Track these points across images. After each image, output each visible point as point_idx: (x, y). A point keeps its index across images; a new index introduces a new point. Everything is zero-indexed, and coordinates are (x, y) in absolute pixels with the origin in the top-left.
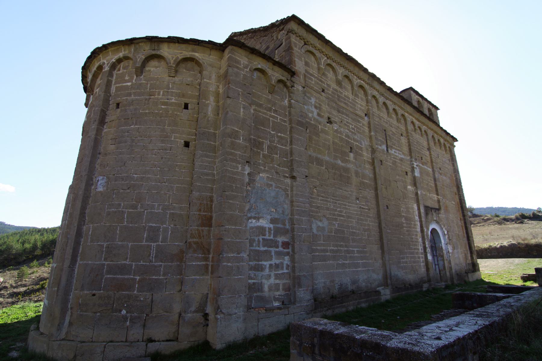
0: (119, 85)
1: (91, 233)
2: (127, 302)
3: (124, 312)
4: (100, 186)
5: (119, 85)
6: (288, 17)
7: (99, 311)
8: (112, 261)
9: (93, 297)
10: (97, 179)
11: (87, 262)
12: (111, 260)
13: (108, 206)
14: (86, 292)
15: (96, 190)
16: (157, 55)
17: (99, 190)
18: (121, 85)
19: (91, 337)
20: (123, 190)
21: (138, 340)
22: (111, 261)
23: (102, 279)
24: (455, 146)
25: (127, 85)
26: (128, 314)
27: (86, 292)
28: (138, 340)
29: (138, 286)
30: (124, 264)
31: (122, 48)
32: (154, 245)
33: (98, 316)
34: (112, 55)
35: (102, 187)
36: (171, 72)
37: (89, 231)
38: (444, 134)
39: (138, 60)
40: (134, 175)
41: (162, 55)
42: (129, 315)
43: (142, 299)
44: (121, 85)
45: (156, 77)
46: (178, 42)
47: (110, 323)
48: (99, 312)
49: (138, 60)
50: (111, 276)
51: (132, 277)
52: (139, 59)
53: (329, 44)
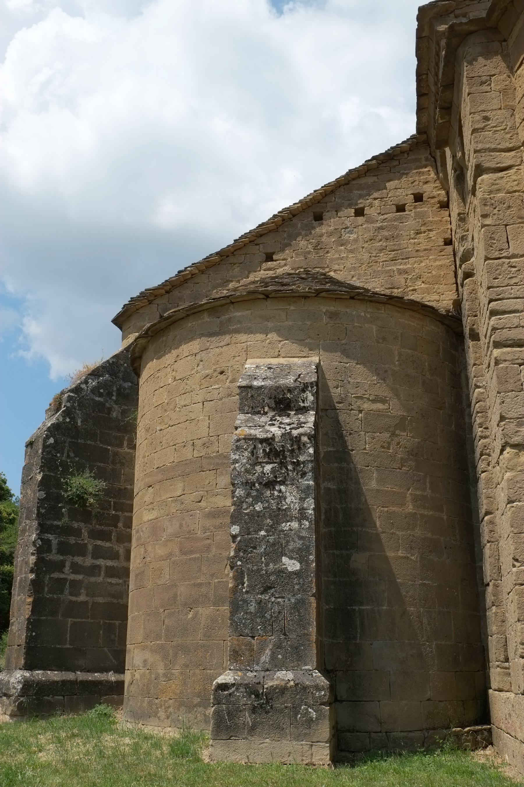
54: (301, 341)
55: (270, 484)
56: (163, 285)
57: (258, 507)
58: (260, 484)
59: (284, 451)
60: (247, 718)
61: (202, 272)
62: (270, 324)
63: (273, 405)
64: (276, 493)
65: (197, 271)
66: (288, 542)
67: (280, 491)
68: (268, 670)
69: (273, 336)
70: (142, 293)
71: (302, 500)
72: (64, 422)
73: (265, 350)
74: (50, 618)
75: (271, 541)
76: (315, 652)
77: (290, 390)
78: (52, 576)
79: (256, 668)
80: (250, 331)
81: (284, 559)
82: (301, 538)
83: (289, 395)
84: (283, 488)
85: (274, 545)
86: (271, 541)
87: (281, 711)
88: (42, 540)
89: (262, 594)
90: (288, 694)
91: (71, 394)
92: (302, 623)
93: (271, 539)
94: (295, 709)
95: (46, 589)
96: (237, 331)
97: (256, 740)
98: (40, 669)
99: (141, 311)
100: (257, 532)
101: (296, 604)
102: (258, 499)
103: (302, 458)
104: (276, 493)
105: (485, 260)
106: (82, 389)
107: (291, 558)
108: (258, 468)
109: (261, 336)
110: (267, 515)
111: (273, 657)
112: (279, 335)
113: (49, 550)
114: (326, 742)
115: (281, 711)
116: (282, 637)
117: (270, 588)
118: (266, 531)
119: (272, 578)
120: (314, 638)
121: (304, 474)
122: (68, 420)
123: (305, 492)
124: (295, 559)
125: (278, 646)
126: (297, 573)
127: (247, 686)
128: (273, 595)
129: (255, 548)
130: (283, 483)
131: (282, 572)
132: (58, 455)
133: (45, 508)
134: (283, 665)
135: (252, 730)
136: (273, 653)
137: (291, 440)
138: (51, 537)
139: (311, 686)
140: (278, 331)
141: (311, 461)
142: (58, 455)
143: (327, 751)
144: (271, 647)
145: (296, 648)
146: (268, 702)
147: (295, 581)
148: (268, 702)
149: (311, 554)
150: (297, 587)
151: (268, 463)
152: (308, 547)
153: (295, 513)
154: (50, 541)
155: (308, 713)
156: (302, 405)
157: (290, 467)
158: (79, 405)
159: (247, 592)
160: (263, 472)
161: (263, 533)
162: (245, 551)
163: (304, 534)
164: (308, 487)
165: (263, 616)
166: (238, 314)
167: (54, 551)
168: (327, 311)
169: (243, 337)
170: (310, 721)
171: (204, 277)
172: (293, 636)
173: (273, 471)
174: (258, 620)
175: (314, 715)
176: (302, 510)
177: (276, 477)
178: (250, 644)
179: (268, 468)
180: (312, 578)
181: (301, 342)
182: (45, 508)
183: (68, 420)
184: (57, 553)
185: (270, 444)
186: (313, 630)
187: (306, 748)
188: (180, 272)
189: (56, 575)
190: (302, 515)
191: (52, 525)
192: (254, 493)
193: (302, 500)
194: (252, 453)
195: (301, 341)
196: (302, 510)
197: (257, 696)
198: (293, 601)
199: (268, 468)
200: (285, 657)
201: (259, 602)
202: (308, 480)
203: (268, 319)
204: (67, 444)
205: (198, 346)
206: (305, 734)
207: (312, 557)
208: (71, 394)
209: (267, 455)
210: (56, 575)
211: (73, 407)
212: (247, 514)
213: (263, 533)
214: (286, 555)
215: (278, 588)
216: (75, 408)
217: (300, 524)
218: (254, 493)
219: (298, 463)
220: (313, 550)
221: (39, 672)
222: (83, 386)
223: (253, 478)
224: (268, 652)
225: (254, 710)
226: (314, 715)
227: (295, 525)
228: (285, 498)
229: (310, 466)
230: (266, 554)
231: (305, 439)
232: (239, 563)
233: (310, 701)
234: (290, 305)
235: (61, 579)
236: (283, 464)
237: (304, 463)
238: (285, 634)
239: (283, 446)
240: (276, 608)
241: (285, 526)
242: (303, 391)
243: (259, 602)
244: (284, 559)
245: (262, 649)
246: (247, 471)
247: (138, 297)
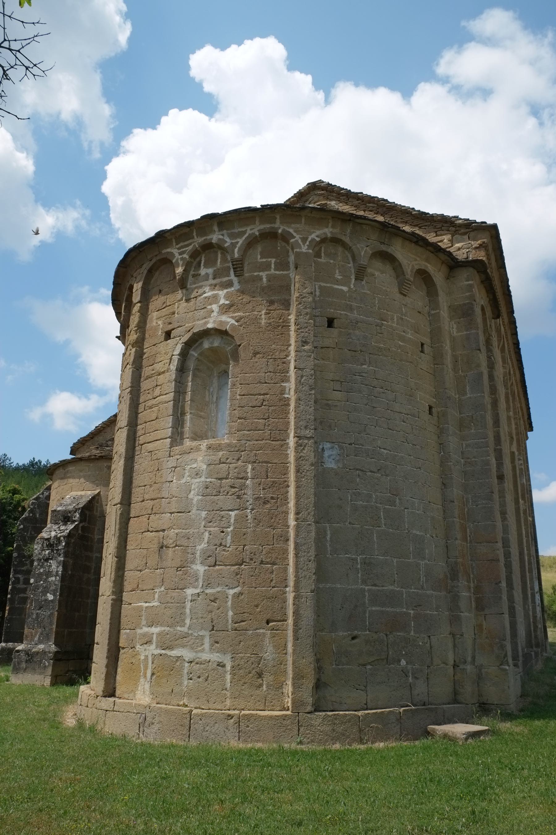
0: (325, 285)
1: (331, 538)
2: (405, 649)
3: (403, 662)
4: (330, 460)
5: (325, 285)
6: (485, 223)
7: (369, 661)
8: (375, 585)
9: (354, 641)
10: (321, 447)
11: (334, 586)
12: (373, 583)
13: (351, 496)
14: (341, 634)
15: (322, 466)
16: (387, 253)
17: (328, 466)
18: (328, 285)
19: (365, 702)
20: (371, 471)
21: (424, 703)
22: (372, 586)
23: (365, 612)
24: (527, 438)
25: (342, 290)
26: (408, 666)
27: (341, 634)
28: (424, 703)
29: (414, 624)
30: (392, 590)
31: (330, 221)
32: (422, 564)
33: (370, 669)
34: (305, 224)
35: (333, 461)
36: (406, 288)
37: (326, 534)
38: (526, 417)
39: (362, 254)
40: (382, 450)
41: (394, 255)
42: (409, 667)
43: (421, 643)
44: (328, 285)
45: (384, 288)
46: (416, 243)
47: (388, 679)
48: (370, 664)
49: (362, 254)
50: (378, 608)
51: (405, 610)
52: (363, 252)
53: (502, 270)
54: (93, 482)
55: (47, 560)
56: (88, 435)
57: (42, 570)
58: (43, 559)
59: (53, 544)
60: (24, 665)
61: (108, 426)
62: (82, 474)
63: (63, 520)
64: (49, 564)
65: (105, 426)
66: (50, 586)
67: (50, 563)
68: (37, 644)
69: (82, 480)
70: (78, 440)
71: (58, 567)
72: (29, 516)
73: (78, 487)
74: (18, 617)
75: (44, 586)
76: (54, 636)
77: (70, 512)
78: (20, 596)
79: (33, 643)
80: (74, 477)
81: (48, 594)
82: (55, 585)
83: (69, 515)
84: (51, 561)
85: (45, 588)
86: (44, 586)
87: (36, 662)
88: (15, 578)
89: (38, 610)
90: (39, 655)
91: (34, 501)
92: (51, 624)
93: (45, 585)
94: (41, 662)
95: (16, 602)
96: (69, 477)
97: (26, 674)
98: (11, 642)
99: (79, 450)
100: (39, 582)
101: (50, 615)
102: (42, 566)
103: (60, 548)
104: (49, 564)
105: (421, 343)
106: (40, 498)
107: (51, 594)
108: (43, 552)
109: (77, 480)
110: (44, 574)
111: (39, 639)
112: (85, 479)
113: (19, 583)
114: (50, 676)
115: (36, 662)
116: (43, 629)
117: (42, 607)
118: (43, 582)
119: (43, 603)
120: (54, 630)
121: (60, 555)
122: (31, 515)
123: (59, 563)
124: (52, 594)
125: (41, 634)
126: (52, 601)
127: (25, 651)
128: (42, 611)
129: (38, 589)
130: (51, 559)
131: (46, 600)
132: (25, 534)
133: (17, 561)
134: (42, 642)
135: (25, 670)
136: (39, 637)
137: (57, 539)
138: (20, 576)
139: (48, 652)
140: (84, 477)
141: (63, 549)
142: (25, 534)
143: (50, 680)
144: (39, 634)
145: (47, 635)
146: (32, 658)
147: (51, 604)
148: (32, 658)
149: (58, 592)
150: (51, 607)
151: (47, 550)
152: (57, 589)
153: (54, 573)
154: (19, 578)
155: (45, 663)
156: (74, 519)
157: (55, 552)
158: (38, 507)
159: (33, 609)
160: (45, 554)
161: (42, 582)
162: (35, 591)
163: (57, 583)
164: (61, 560)
165: (38, 620)
166: (71, 468)
167: (21, 583)
168: (107, 465)
169: (71, 480)
170: (45, 667)
171: (109, 428)
172: (47, 629)
173: (49, 553)
174: (36, 622)
175: (47, 664)
176: (57, 571)
177: (49, 556)
178: (31, 633)
179: (47, 552)
180: (57, 603)
181: (93, 482)
182: (17, 561)
183: (31, 515)
184: (23, 584)
185: (49, 541)
186: (54, 626)
187: (43, 678)
188: (96, 427)
189: (22, 595)
190: (57, 575)
191: (20, 570)
192: (41, 564)
193: (58, 567)
194: (42, 545)
195: (93, 482)
196: (57, 571)
197: (28, 655)
198: (49, 613)
199: (47, 552)
200: (43, 639)
201: (37, 614)
202: (61, 558)
203: (81, 471)
204: (30, 528)
205: (57, 484)
206: (43, 672)
207: (58, 594)
208: (34, 501)
209: (47, 546)
210: (22, 595)
211: (34, 508)
212: (37, 574)
213: (42, 582)
214: (49, 592)
215: (45, 608)
216: (35, 508)
217: (56, 578)
218: (41, 564)
219: (58, 550)
220: (59, 590)
221: (11, 644)
222: (41, 496)
223: (41, 557)
224: (38, 636)
225: (26, 661)
226: (47, 664)
227: (53, 578)
228: (52, 566)
229: (62, 551)
230: (42, 592)
231: (62, 538)
232: (32, 596)
233: (46, 658)
234: (91, 463)
235: (24, 597)
236: (52, 551)
237: (60, 549)
238: (45, 628)
239: (53, 542)
240: (43, 617)
241: (50, 579)
242: (75, 512)
243: (37, 614)
244: (48, 594)
245: (36, 635)
246: (39, 554)
247: (77, 442)
